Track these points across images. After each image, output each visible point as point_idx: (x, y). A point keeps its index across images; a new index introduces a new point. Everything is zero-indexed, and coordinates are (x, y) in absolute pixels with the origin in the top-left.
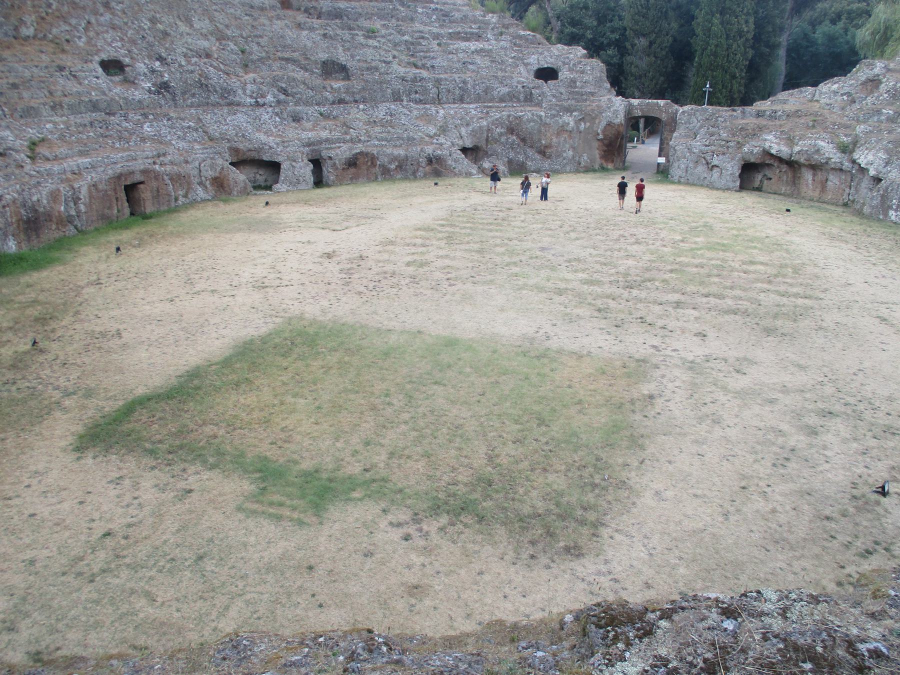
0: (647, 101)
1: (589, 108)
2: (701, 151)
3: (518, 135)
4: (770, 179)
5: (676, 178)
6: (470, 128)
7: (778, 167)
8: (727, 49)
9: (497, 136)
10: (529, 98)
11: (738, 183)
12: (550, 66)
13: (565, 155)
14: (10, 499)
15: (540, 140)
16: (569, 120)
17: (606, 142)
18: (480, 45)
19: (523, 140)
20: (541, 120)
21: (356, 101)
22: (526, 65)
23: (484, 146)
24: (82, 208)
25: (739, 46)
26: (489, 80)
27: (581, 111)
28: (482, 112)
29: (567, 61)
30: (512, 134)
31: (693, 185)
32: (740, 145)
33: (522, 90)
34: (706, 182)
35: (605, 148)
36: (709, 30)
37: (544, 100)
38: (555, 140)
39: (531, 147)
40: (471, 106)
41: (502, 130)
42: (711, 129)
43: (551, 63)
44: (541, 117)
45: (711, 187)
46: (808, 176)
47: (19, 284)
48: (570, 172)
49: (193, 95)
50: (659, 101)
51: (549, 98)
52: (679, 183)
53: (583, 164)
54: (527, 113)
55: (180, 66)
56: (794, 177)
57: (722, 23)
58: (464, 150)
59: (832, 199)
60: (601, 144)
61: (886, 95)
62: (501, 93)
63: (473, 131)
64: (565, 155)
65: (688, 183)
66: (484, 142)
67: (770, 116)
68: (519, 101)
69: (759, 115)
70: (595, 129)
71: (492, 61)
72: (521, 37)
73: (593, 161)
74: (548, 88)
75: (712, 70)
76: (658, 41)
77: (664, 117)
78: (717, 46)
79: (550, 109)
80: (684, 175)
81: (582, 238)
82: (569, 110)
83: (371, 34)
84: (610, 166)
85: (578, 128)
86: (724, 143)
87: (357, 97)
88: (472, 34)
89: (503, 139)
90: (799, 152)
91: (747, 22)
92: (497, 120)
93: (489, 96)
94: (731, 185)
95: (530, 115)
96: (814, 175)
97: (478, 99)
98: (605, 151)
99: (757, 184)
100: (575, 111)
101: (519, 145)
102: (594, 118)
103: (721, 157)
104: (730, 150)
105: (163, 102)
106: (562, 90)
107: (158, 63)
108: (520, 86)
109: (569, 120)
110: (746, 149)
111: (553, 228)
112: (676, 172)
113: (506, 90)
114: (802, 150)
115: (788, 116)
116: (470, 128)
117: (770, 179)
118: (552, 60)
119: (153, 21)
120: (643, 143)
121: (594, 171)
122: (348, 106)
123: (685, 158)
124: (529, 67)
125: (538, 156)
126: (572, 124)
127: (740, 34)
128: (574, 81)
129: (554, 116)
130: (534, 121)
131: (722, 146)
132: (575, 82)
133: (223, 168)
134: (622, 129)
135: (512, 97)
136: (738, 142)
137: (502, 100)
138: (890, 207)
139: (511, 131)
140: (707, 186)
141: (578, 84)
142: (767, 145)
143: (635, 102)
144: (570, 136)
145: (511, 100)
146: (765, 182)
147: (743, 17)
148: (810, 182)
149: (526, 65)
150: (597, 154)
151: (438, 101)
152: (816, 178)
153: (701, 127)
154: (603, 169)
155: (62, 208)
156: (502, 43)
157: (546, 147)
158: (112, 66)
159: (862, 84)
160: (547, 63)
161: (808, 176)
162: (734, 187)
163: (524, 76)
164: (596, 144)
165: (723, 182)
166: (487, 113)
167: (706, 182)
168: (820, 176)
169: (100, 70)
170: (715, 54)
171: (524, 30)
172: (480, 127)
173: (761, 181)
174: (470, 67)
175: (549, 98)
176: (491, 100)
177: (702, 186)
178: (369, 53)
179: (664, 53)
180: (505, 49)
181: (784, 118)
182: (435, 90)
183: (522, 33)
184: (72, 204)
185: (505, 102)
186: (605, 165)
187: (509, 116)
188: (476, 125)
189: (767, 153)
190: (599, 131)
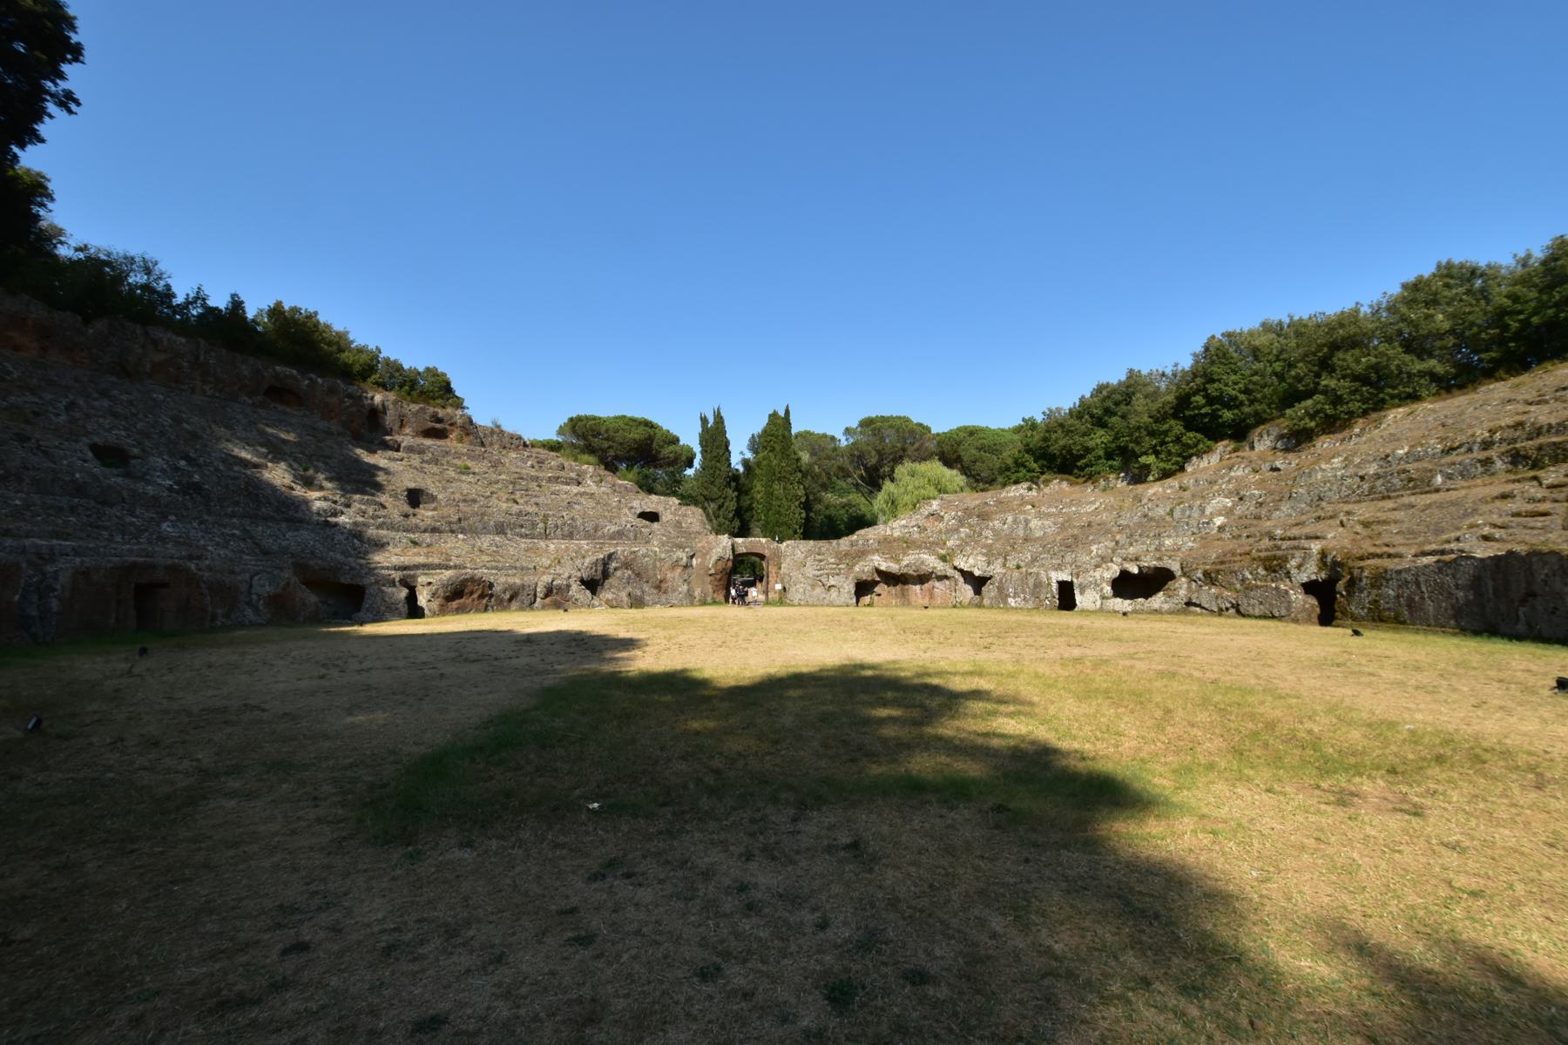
14: (242, 1002)
18: (581, 489)
19: (638, 575)
21: (452, 532)
24: (54, 605)
45: (831, 605)
46: (1372, 787)
47: (306, 470)
49: (237, 504)
55: (217, 470)
58: (583, 582)
77: (766, 553)
82: (680, 547)
83: (466, 470)
87: (455, 527)
97: (588, 536)
105: (190, 505)
107: (183, 463)
112: (795, 594)
113: (614, 528)
119: (177, 420)
122: (444, 535)
133: (288, 584)
138: (1008, 596)
143: (740, 540)
150: (710, 588)
151: (546, 536)
155: (17, 598)
158: (111, 455)
163: (629, 519)
169: (90, 454)
178: (465, 488)
182: (541, 525)
184: (35, 598)
189: (879, 572)
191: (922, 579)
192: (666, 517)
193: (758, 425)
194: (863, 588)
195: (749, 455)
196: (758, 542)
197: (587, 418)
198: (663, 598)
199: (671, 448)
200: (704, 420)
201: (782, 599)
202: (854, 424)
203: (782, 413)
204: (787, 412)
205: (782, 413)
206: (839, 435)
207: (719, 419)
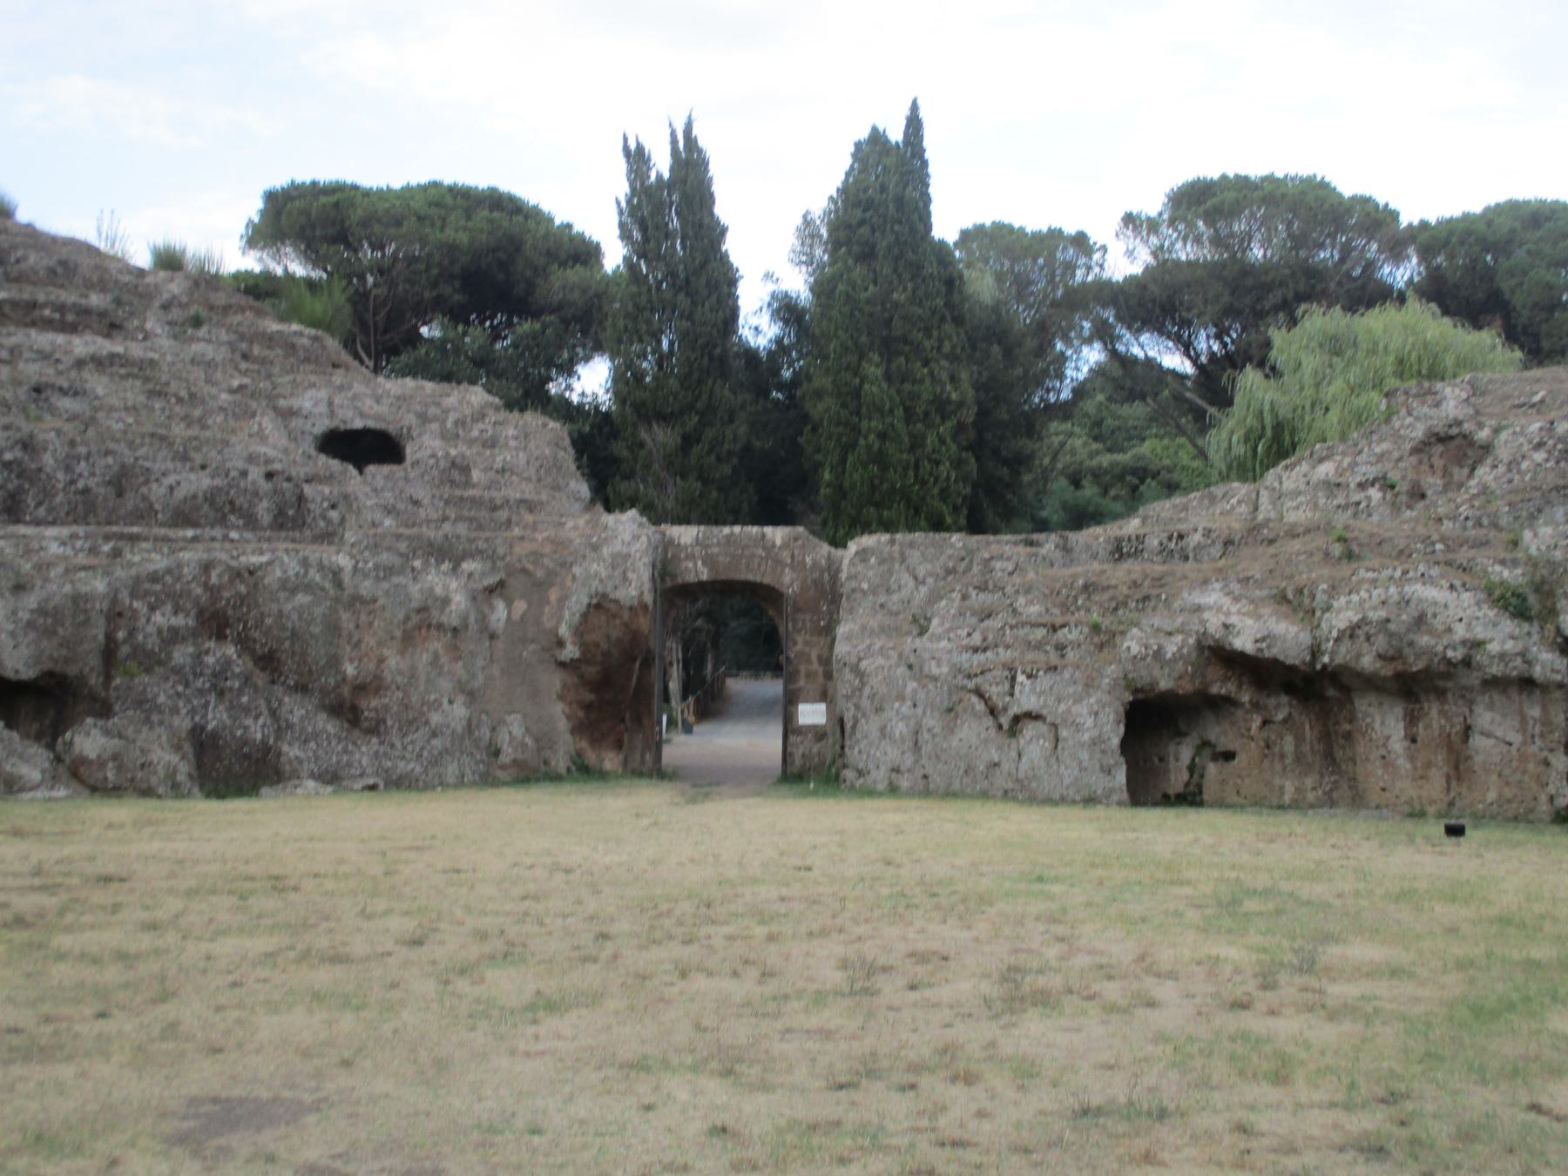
0: (726, 530)
1: (521, 549)
2: (957, 670)
3: (244, 642)
4: (1229, 756)
5: (879, 777)
6: (31, 601)
7: (1256, 706)
8: (912, 449)
9: (153, 643)
10: (291, 516)
11: (1121, 777)
12: (371, 424)
13: (435, 718)
15: (334, 662)
16: (451, 588)
17: (591, 671)
19: (268, 661)
20: (339, 584)
22: (287, 414)
23: (94, 680)
25: (942, 442)
26: (131, 445)
27: (491, 557)
28: (93, 551)
29: (432, 411)
30: (221, 637)
31: (949, 794)
32: (1103, 638)
33: (265, 486)
34: (1001, 781)
35: (589, 697)
36: (857, 393)
37: (351, 520)
38: (394, 661)
39: (302, 688)
40: (51, 532)
41: (179, 621)
42: (979, 599)
43: (378, 418)
44: (336, 575)
45: (1023, 793)
46: (1385, 724)
48: (460, 783)
50: (768, 530)
51: (369, 516)
52: (893, 790)
53: (508, 754)
54: (277, 559)
56: (1326, 737)
57: (888, 377)
59: (1501, 801)
60: (572, 680)
61: (1539, 456)
62: (180, 494)
63: (41, 611)
64: (435, 718)
65: (925, 790)
66: (94, 661)
67: (1163, 548)
68: (251, 522)
69: (1119, 552)
70: (548, 624)
71: (151, 394)
72: (270, 340)
73: (544, 741)
74: (369, 486)
75: (878, 505)
76: (709, 434)
77: (789, 582)
78: (883, 436)
79: (375, 547)
80: (908, 760)
81: (593, 999)
82: (446, 553)
84: (611, 761)
85: (483, 619)
86: (1040, 633)
88: (86, 312)
89: (181, 655)
90: (1351, 632)
91: (953, 379)
92: (154, 578)
93: (130, 501)
94: (1099, 783)
95: (293, 567)
96: (1412, 719)
97: (83, 509)
98: (588, 707)
99: (1177, 779)
100: (465, 556)
101: (247, 679)
102: (542, 586)
103: (1045, 681)
104: (1071, 655)
106: (421, 493)
108: (256, 473)
109: (451, 588)
110: (1132, 644)
111: (359, 947)
112: (875, 749)
113: (196, 483)
114: (1364, 621)
115: (1228, 543)
116: (31, 601)
117: (1229, 756)
118: (383, 409)
120: (688, 729)
121: (555, 778)
123: (901, 698)
124: (295, 423)
125: (328, 725)
126: (459, 601)
127: (942, 407)
128: (460, 468)
129: (390, 571)
130: (309, 588)
131: (1039, 646)
132: (466, 470)
134: (644, 623)
135: (223, 508)
136: (1096, 628)
137: (183, 516)
139: (214, 623)
140: (1006, 795)
141: (476, 475)
142: (1213, 623)
143: (686, 534)
144: (454, 648)
145: (222, 521)
146: (1212, 769)
147: (944, 363)
148: (1398, 744)
149: (287, 414)
150: (559, 716)
152: (1421, 730)
153: (935, 597)
154: (584, 771)
156: (197, 348)
157: (361, 688)
159: (1416, 450)
160: (362, 415)
161: (1385, 724)
162: (1108, 794)
164: (554, 681)
165: (1069, 773)
166: (116, 553)
167: (1001, 781)
168: (1435, 717)
170: (880, 459)
171: (282, 319)
172: (76, 599)
173: (1192, 768)
174: (65, 403)
175: (369, 516)
176: (139, 516)
177: (985, 795)
179: (726, 469)
180: (210, 365)
181: (1216, 551)
183: (274, 327)
185: (195, 525)
186: (591, 757)
187: (207, 567)
188: (57, 589)
189: (1221, 656)
190: (564, 631)
191: (1417, 684)
192: (424, 447)
193: (820, 182)
194: (1152, 721)
195: (797, 284)
196: (776, 550)
197: (315, 190)
198: (365, 753)
199: (574, 274)
200: (637, 159)
201: (814, 768)
202: (1152, 204)
203: (896, 134)
204: (914, 124)
205: (896, 134)
206: (1103, 230)
207: (691, 162)
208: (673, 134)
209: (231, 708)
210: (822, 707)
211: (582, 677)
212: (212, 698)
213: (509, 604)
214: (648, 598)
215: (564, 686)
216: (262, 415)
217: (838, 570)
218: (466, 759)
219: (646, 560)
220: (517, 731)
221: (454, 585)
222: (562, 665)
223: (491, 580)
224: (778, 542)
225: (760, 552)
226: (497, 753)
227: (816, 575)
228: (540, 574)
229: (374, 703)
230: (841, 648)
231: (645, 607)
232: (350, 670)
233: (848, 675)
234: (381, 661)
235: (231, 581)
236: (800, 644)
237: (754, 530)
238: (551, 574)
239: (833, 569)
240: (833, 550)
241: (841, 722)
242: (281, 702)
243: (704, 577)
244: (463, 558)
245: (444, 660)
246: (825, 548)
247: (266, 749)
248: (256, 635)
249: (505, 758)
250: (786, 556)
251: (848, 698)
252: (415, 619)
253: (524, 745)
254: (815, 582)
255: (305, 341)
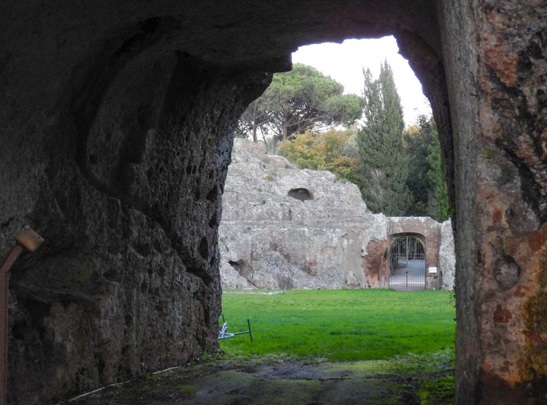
0: (408, 218)
3: (281, 251)
12: (303, 187)
15: (304, 257)
19: (287, 257)
23: (249, 261)
30: (276, 250)
35: (370, 266)
39: (295, 263)
40: (231, 222)
50: (420, 218)
66: (249, 256)
77: (425, 233)
85: (341, 245)
124: (282, 187)
126: (336, 240)
132: (333, 201)
139: (274, 247)
143: (396, 219)
150: (362, 271)
157: (311, 264)
160: (299, 184)
164: (361, 261)
199: (333, 99)
208: (382, 65)
209: (280, 269)
210: (436, 268)
211: (368, 260)
212: (275, 266)
213: (348, 240)
214: (386, 238)
215: (363, 263)
216: (274, 186)
217: (440, 230)
218: (338, 283)
219: (385, 227)
220: (352, 275)
221: (334, 235)
222: (363, 257)
223: (344, 234)
224: (423, 221)
225: (417, 224)
226: (346, 282)
227: (434, 231)
228: (356, 232)
229: (314, 267)
230: (441, 253)
231: (386, 241)
232: (308, 259)
233: (443, 260)
234: (316, 256)
235: (278, 235)
236: (429, 251)
237: (416, 218)
238: (359, 232)
239: (439, 230)
240: (439, 223)
241: (441, 272)
242: (291, 267)
243: (401, 232)
244: (336, 228)
245: (332, 256)
246: (436, 223)
247: (289, 279)
248: (284, 250)
249: (349, 283)
250: (425, 225)
251: (443, 266)
252: (324, 245)
253: (353, 279)
254: (434, 233)
255: (279, 160)
